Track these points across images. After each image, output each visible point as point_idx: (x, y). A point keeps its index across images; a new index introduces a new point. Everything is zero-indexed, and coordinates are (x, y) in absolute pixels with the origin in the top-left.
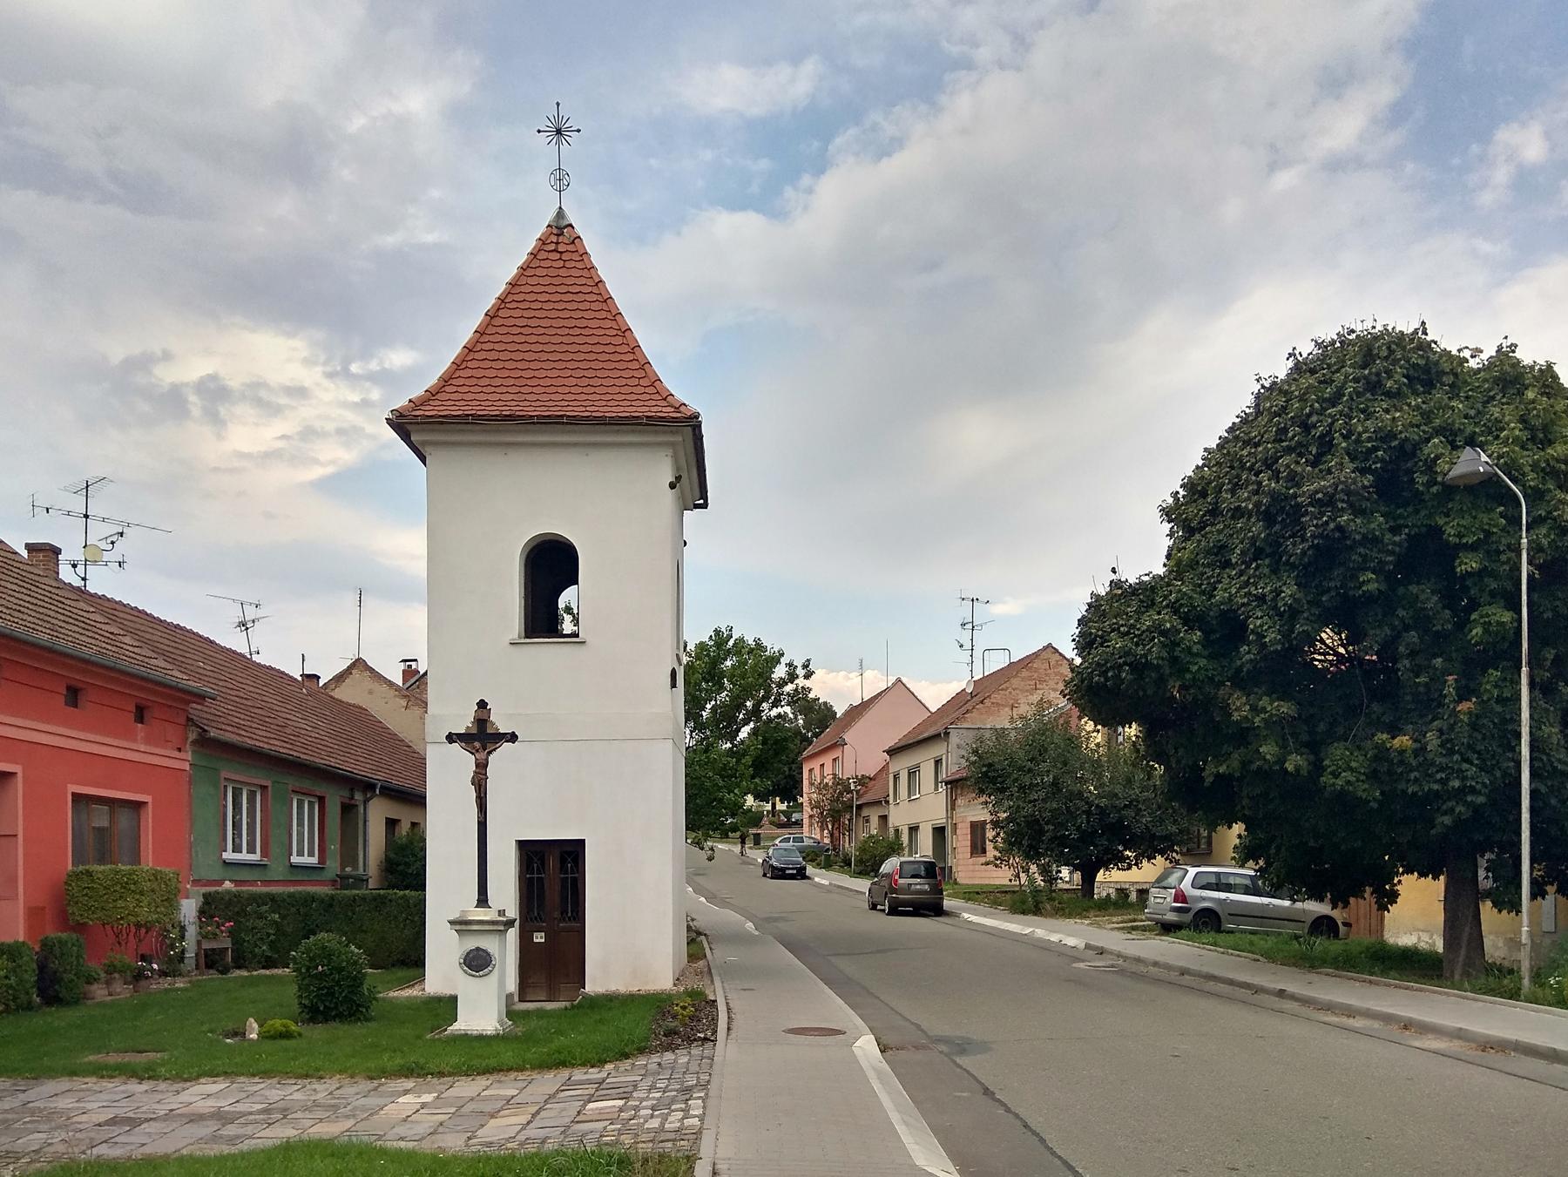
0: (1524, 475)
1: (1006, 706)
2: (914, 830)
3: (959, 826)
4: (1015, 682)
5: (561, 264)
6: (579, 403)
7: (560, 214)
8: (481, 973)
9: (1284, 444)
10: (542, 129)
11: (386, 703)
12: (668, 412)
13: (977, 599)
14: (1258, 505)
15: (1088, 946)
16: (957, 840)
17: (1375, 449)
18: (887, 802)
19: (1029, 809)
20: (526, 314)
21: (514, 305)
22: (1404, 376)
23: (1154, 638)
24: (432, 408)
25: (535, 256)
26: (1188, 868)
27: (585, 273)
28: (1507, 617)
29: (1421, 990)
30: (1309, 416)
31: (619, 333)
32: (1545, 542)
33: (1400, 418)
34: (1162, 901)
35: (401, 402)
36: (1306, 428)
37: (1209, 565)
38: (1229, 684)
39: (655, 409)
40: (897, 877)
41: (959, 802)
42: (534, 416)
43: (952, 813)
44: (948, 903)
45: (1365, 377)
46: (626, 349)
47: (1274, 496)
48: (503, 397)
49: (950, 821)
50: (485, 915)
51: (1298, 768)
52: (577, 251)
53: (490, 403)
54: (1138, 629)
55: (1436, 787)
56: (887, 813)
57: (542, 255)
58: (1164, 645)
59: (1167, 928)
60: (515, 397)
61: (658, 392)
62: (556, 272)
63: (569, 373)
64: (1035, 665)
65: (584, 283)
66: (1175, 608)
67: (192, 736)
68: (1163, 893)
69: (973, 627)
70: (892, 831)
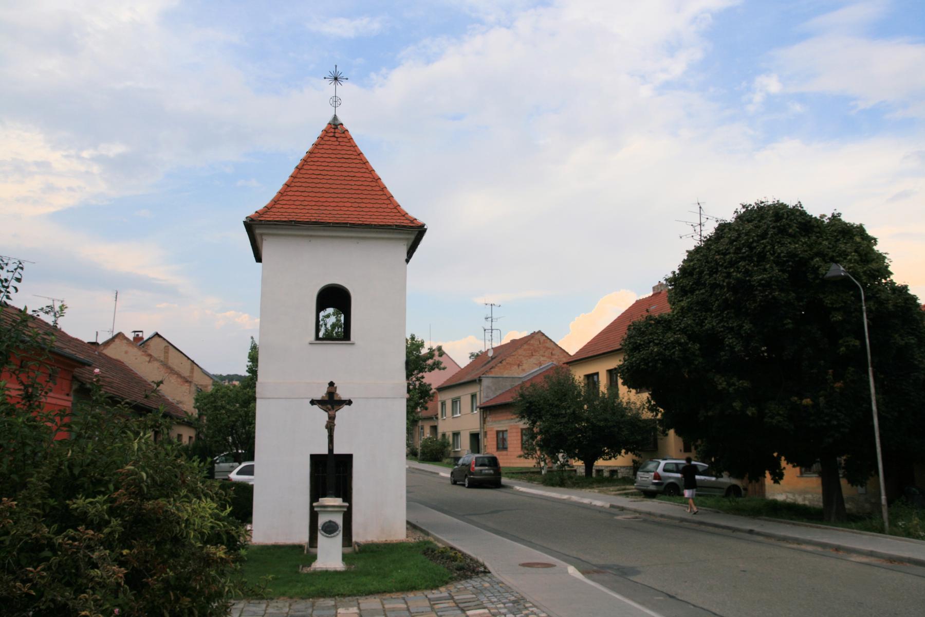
0: (860, 277)
2: (456, 435)
4: (520, 351)
5: (337, 143)
7: (335, 118)
8: (332, 535)
9: (740, 255)
11: (136, 359)
12: (406, 223)
14: (729, 283)
15: (612, 506)
17: (788, 261)
18: (437, 418)
19: (558, 427)
20: (320, 168)
21: (312, 163)
22: (797, 228)
23: (675, 347)
26: (660, 461)
27: (352, 149)
28: (857, 343)
29: (827, 529)
30: (752, 243)
32: (873, 308)
33: (797, 247)
34: (646, 479)
35: (251, 212)
36: (751, 248)
37: (698, 310)
38: (714, 370)
39: (399, 221)
40: (474, 466)
41: (488, 419)
44: (504, 480)
45: (778, 227)
46: (378, 188)
47: (738, 279)
48: (310, 211)
50: (335, 502)
51: (753, 413)
53: (303, 215)
54: (665, 342)
55: (825, 424)
56: (436, 424)
57: (326, 138)
58: (680, 351)
59: (649, 494)
60: (317, 212)
61: (399, 212)
63: (347, 200)
64: (532, 342)
66: (683, 331)
67: (75, 387)
68: (646, 475)
70: (440, 436)
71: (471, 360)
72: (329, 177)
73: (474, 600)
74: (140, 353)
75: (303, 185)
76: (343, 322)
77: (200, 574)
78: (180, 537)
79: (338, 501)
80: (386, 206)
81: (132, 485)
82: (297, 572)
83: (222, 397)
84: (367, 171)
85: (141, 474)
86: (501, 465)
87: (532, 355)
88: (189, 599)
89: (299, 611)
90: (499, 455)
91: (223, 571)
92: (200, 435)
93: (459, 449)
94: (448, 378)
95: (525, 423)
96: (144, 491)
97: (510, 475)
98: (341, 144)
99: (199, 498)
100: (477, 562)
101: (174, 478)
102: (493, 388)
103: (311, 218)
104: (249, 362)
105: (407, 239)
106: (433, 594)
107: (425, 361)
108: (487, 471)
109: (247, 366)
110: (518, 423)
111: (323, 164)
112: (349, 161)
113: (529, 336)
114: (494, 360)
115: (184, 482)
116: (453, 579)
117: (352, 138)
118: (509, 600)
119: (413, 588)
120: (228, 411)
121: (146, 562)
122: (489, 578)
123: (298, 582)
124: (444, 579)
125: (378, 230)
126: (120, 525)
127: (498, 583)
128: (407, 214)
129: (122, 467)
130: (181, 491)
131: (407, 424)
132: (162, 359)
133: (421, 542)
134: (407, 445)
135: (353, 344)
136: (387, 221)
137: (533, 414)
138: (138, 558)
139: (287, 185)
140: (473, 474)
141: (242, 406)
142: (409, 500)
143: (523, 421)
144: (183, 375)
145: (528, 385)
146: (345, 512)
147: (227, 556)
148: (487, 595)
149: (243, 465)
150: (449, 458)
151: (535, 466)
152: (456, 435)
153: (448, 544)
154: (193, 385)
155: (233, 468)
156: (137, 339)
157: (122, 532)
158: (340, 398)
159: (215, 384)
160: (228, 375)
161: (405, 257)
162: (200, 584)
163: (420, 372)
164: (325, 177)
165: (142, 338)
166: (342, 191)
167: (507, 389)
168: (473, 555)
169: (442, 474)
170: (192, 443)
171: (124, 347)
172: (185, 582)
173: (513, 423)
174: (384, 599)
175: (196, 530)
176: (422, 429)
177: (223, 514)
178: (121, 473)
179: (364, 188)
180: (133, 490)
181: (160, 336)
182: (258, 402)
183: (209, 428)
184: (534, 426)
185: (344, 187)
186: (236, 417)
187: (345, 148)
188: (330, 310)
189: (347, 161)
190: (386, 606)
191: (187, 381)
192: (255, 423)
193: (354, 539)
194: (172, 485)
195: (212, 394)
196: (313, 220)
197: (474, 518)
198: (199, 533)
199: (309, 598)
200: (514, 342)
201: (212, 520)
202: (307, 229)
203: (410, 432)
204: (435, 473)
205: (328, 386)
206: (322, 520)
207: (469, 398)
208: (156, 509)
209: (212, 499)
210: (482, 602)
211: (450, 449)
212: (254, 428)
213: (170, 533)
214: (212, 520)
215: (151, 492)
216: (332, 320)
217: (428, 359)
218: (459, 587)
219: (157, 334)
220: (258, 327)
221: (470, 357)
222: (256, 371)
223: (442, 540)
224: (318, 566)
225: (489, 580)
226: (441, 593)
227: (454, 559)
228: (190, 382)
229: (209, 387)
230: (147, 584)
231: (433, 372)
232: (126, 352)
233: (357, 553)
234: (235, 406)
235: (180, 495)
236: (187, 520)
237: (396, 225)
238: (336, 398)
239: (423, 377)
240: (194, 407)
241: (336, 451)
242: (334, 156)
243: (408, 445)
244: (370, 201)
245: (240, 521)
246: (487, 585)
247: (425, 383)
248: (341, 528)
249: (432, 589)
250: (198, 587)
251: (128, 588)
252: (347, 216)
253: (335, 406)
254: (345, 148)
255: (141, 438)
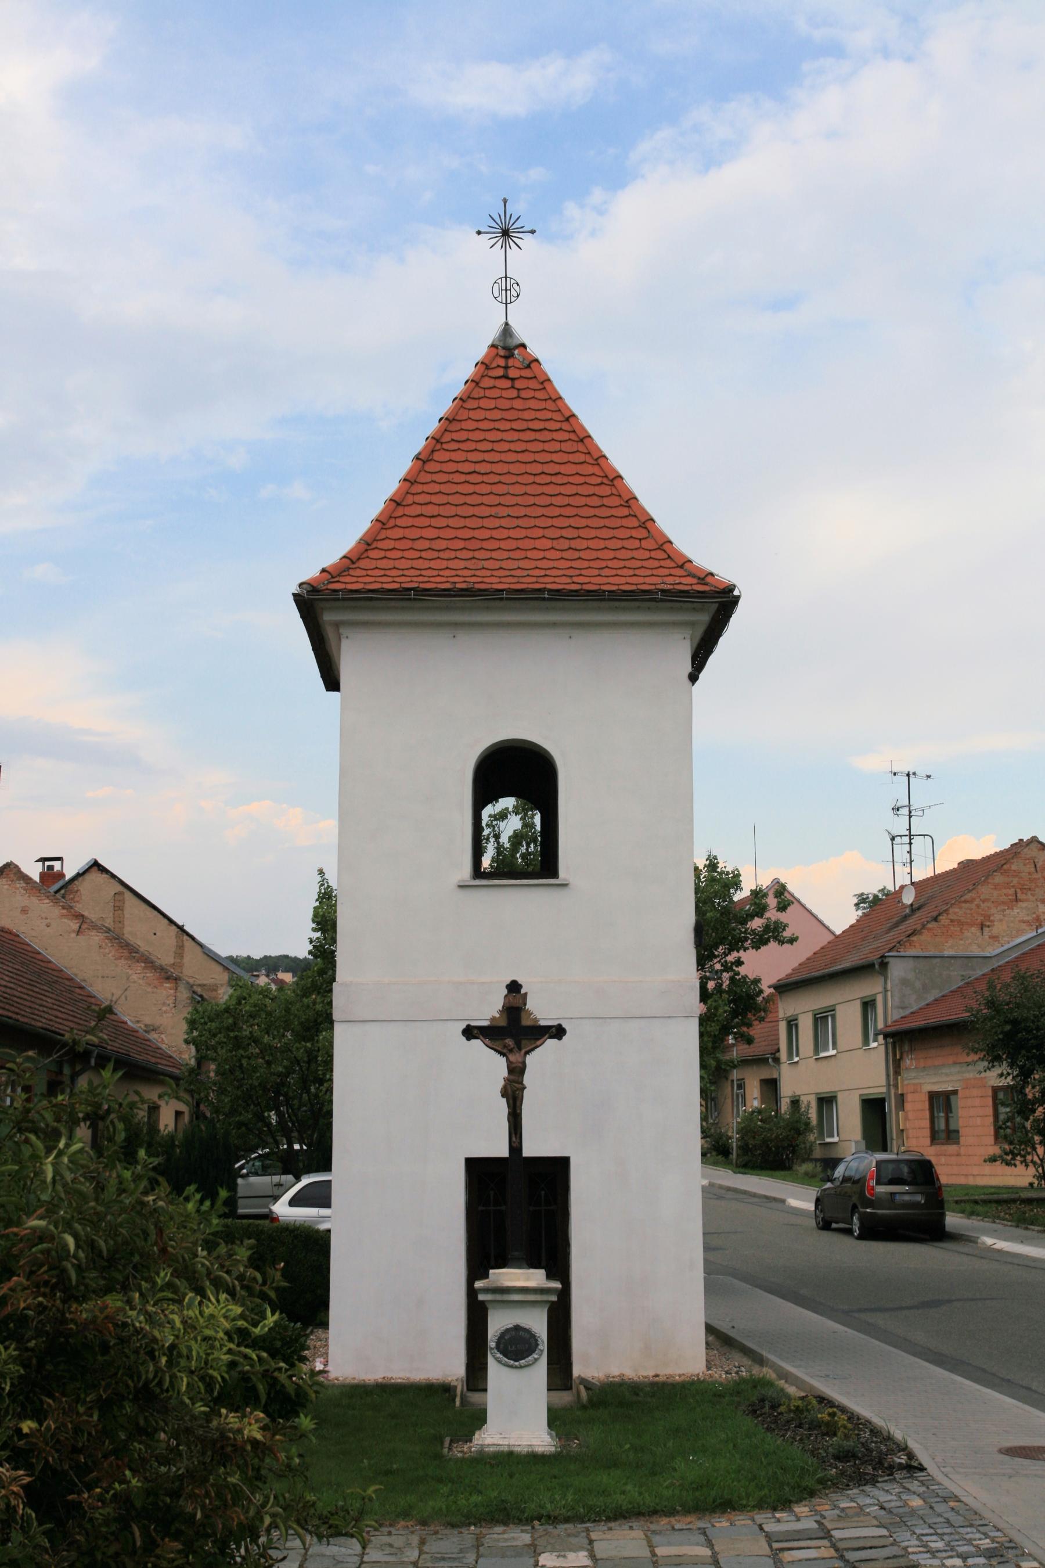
1: (972, 925)
2: (826, 1102)
3: (909, 1098)
4: (985, 891)
5: (514, 393)
6: (560, 573)
7: (507, 330)
10: (482, 230)
12: (687, 583)
13: (914, 774)
16: (906, 1119)
18: (777, 1060)
20: (472, 457)
21: (454, 446)
24: (354, 579)
25: (477, 384)
27: (550, 405)
31: (605, 481)
35: (310, 572)
39: (670, 580)
40: (873, 1183)
41: (907, 1062)
42: (502, 590)
43: (896, 1079)
44: (953, 1220)
46: (615, 502)
49: (893, 1091)
50: (528, 1279)
52: (535, 377)
53: (435, 573)
57: (487, 383)
60: (468, 564)
62: (507, 404)
63: (540, 533)
64: (1014, 867)
65: (549, 417)
69: (910, 812)
70: (785, 1105)
71: (860, 913)
72: (497, 479)
73: (882, 1542)
74: (57, 911)
75: (435, 499)
76: (538, 828)
77: (206, 1480)
78: (158, 1390)
79: (534, 1278)
80: (637, 544)
81: (41, 1266)
82: (438, 1456)
83: (252, 1016)
84: (588, 459)
85: (63, 1238)
86: (944, 1180)
87: (1017, 900)
88: (177, 1545)
89: (444, 1559)
90: (937, 1155)
91: (258, 1470)
92: (202, 1107)
93: (836, 1139)
94: (802, 959)
95: (1001, 1075)
96: (70, 1279)
97: (968, 1207)
98: (523, 394)
99: (200, 1291)
100: (889, 1438)
101: (140, 1243)
102: (918, 985)
103: (456, 579)
104: (314, 930)
105: (692, 624)
106: (778, 1521)
107: (744, 922)
108: (907, 1198)
109: (311, 942)
110: (983, 1075)
111: (482, 446)
112: (546, 436)
113: (1007, 851)
114: (918, 914)
115: (164, 1251)
116: (828, 1485)
117: (549, 380)
118: (977, 1546)
119: (726, 1505)
120: (265, 1049)
121: (75, 1450)
122: (923, 1483)
123: (440, 1480)
124: (804, 1484)
125: (617, 604)
126: (14, 1360)
127: (945, 1500)
128: (690, 561)
129: (19, 1223)
130: (158, 1274)
131: (702, 1078)
132: (109, 923)
133: (743, 1381)
134: (703, 1132)
135: (565, 885)
136: (641, 580)
137: (1023, 1052)
138: (58, 1441)
139: (395, 502)
140: (870, 1203)
141: (300, 1037)
142: (710, 1268)
143: (998, 1071)
144: (158, 963)
145: (1007, 977)
146: (553, 1303)
147: (268, 1436)
148: (918, 1531)
149: (305, 1181)
150: (811, 1160)
151: (1031, 1184)
152: (826, 1102)
153: (812, 1387)
154: (182, 988)
155: (282, 1188)
156: (50, 876)
157: (21, 1377)
158: (536, 1020)
159: (234, 982)
160: (265, 957)
161: (688, 668)
162: (203, 1507)
163: (731, 950)
164: (486, 478)
165: (61, 875)
166: (528, 511)
167: (954, 987)
168: (878, 1421)
169: (793, 1202)
170: (180, 1126)
171: (21, 898)
172: (168, 1500)
173: (970, 1074)
174: (654, 1532)
175: (192, 1372)
176: (740, 1087)
177: (257, 1331)
178: (16, 1235)
179: (582, 501)
180: (46, 1277)
181: (103, 870)
182: (338, 1030)
183: (222, 1091)
184: (1025, 1083)
185: (532, 500)
186: (285, 1063)
187: (532, 404)
188: (508, 802)
189: (537, 435)
190: (659, 1551)
191: (168, 976)
192: (331, 1080)
193: (577, 1371)
194: (136, 1258)
195: (227, 1010)
196: (458, 586)
197: (879, 1320)
198: (202, 1379)
199: (469, 1525)
200: (967, 866)
201: (232, 1346)
202: (448, 609)
203: (709, 1096)
204: (775, 1200)
205: (505, 992)
206: (497, 1323)
207: (856, 1009)
208: (99, 1320)
209: (232, 1293)
210: (905, 1548)
211: (812, 1137)
212: (330, 1090)
213: (131, 1378)
214: (232, 1346)
215: (87, 1281)
216: (513, 824)
217: (751, 916)
218: (843, 1505)
219: (96, 865)
220: (334, 839)
221: (857, 905)
222: (333, 953)
223: (797, 1378)
224: (488, 1441)
225: (922, 1489)
226: (798, 1519)
227: (830, 1429)
228: (177, 979)
229: (221, 991)
230: (77, 1505)
231: (763, 948)
232: (24, 911)
233: (584, 1407)
234: (283, 1036)
235: (154, 1283)
236: (173, 1347)
237: (663, 591)
238: (525, 1022)
239: (739, 963)
240: (187, 1042)
241: (527, 1152)
242: (507, 426)
243: (705, 1133)
244: (589, 522)
245: (299, 1325)
246: (916, 1502)
247: (745, 977)
248: (543, 1345)
249: (775, 1509)
250: (199, 1515)
251: (34, 1515)
252: (543, 573)
253: (524, 1042)
254: (532, 404)
255: (61, 1153)
